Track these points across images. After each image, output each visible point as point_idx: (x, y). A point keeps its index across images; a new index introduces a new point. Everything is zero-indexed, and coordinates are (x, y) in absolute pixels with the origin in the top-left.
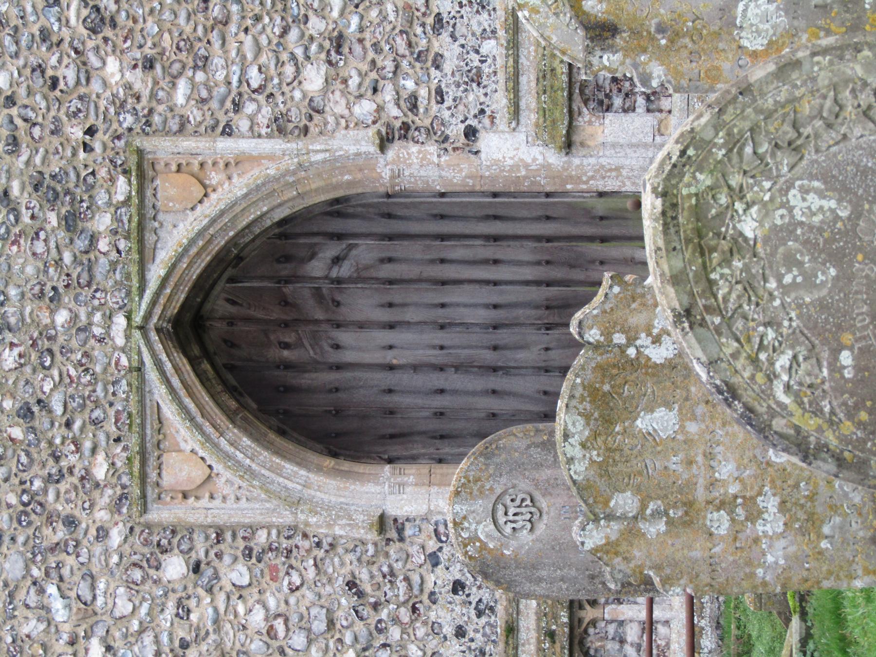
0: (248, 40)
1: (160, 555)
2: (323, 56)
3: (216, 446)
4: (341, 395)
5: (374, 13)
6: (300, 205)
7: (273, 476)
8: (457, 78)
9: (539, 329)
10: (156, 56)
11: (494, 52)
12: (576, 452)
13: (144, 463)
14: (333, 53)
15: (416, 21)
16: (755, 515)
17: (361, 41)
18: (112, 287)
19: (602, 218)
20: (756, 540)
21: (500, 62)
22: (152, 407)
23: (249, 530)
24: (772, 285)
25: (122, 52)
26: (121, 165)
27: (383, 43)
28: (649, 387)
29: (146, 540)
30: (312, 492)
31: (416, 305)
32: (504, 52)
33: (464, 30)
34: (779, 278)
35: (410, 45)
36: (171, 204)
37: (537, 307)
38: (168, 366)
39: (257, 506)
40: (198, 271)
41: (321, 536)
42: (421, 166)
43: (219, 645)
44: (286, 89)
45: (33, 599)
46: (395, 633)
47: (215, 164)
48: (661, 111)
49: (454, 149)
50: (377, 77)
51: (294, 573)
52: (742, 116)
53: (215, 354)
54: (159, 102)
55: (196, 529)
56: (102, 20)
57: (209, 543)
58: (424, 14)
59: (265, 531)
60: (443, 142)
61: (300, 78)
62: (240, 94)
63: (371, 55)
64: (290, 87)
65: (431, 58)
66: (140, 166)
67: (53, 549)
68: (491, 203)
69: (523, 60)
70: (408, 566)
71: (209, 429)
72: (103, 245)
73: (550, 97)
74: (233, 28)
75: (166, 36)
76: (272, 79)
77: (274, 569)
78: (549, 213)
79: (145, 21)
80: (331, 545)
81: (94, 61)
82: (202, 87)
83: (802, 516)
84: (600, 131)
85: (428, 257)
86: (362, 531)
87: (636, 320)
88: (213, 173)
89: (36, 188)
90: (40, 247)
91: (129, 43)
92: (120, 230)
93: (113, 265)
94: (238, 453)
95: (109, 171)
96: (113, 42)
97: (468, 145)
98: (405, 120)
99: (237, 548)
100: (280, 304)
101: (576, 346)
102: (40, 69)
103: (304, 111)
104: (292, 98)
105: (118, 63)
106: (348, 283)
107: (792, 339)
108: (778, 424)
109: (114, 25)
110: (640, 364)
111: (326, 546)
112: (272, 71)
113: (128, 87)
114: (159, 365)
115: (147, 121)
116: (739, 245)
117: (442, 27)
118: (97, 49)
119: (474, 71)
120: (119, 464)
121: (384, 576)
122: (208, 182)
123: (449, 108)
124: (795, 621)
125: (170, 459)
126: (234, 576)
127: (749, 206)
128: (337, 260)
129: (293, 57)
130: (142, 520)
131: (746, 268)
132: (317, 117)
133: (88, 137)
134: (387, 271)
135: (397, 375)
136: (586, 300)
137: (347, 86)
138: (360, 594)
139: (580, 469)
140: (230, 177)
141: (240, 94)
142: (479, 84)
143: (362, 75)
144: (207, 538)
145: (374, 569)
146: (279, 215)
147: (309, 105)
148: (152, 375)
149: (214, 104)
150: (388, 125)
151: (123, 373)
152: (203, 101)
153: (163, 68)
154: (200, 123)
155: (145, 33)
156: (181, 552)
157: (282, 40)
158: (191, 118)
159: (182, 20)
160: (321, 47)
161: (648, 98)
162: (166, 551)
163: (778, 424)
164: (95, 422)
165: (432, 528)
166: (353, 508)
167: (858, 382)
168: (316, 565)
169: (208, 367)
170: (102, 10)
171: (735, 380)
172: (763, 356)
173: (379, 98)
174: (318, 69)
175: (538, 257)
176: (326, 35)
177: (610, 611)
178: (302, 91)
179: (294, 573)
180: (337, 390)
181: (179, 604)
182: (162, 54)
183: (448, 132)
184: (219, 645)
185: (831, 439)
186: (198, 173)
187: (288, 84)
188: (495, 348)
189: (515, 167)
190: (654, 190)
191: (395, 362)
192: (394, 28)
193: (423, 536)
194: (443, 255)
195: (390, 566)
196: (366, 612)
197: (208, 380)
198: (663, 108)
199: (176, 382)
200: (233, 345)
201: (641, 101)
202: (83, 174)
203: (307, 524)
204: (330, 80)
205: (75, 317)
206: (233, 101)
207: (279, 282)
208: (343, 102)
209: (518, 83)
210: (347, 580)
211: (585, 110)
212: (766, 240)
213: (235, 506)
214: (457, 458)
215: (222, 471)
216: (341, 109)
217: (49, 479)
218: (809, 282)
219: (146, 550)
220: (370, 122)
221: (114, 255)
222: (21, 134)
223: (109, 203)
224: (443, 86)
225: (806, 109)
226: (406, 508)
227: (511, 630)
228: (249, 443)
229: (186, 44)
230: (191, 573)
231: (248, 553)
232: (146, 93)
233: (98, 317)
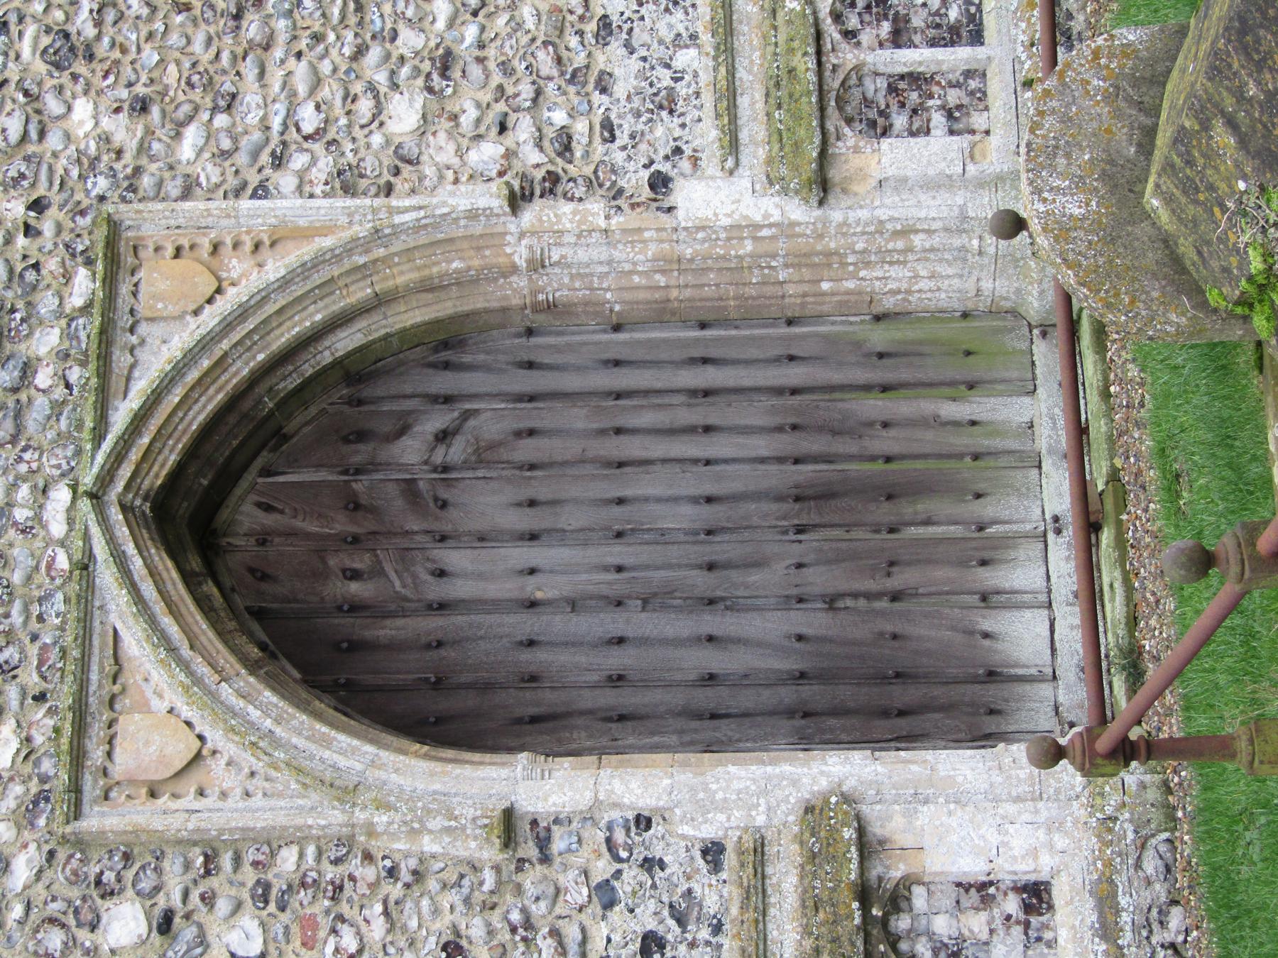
1: (99, 901)
2: (420, 82)
3: (214, 696)
4: (447, 653)
5: (502, 20)
7: (312, 747)
8: (636, 102)
9: (786, 532)
10: (153, 96)
11: (695, 65)
13: (80, 728)
14: (435, 76)
15: (568, 30)
17: (480, 60)
18: (53, 441)
19: (881, 356)
21: (705, 78)
22: (103, 635)
23: (265, 849)
25: (100, 92)
26: (83, 252)
27: (516, 63)
29: (75, 873)
30: (382, 775)
31: (576, 501)
32: (711, 63)
33: (646, 37)
35: (559, 61)
36: (160, 306)
37: (780, 498)
38: (137, 564)
39: (282, 803)
40: (201, 418)
41: (397, 857)
44: (358, 132)
47: (236, 245)
48: (973, 132)
49: (633, 206)
50: (506, 109)
51: (346, 931)
53: (233, 590)
54: (153, 159)
55: (168, 850)
56: (72, 49)
57: (191, 875)
58: (582, 18)
59: (295, 849)
60: (614, 198)
61: (382, 118)
62: (284, 144)
63: (497, 78)
64: (366, 131)
65: (592, 80)
66: (111, 243)
68: (697, 340)
69: (741, 73)
70: (558, 910)
71: (202, 669)
72: (43, 378)
73: (788, 111)
74: (278, 53)
75: (172, 68)
76: (337, 120)
77: (309, 924)
78: (793, 352)
79: (139, 50)
80: (415, 873)
81: (53, 105)
82: (222, 135)
84: (873, 163)
85: (595, 426)
86: (473, 844)
88: (234, 261)
91: (111, 79)
92: (73, 352)
93: (57, 408)
94: (251, 709)
95: (63, 259)
96: (85, 79)
97: (655, 200)
98: (552, 168)
99: (243, 884)
100: (346, 508)
103: (386, 163)
104: (368, 146)
105: (91, 106)
106: (461, 469)
109: (90, 57)
111: (406, 876)
112: (338, 110)
113: (106, 139)
115: (131, 185)
117: (611, 33)
118: (60, 89)
119: (664, 93)
120: (39, 739)
121: (514, 930)
122: (224, 275)
123: (624, 148)
125: (130, 725)
129: (372, 88)
130: (68, 829)
132: (406, 170)
133: (32, 214)
134: (527, 450)
135: (545, 618)
137: (457, 125)
141: (284, 144)
142: (671, 112)
143: (483, 108)
144: (187, 866)
145: (495, 918)
147: (395, 152)
148: (106, 575)
149: (242, 159)
150: (524, 176)
151: (58, 582)
152: (226, 155)
153: (163, 112)
154: (218, 186)
155: (138, 66)
156: (138, 894)
157: (354, 66)
158: (203, 180)
159: (197, 47)
160: (417, 71)
161: (950, 115)
162: (112, 893)
165: (601, 836)
166: (454, 800)
168: (386, 913)
169: (215, 590)
170: (74, 37)
173: (509, 140)
174: (411, 101)
175: (778, 420)
176: (425, 54)
178: (384, 135)
179: (346, 931)
180: (440, 644)
182: (163, 94)
183: (622, 183)
187: (362, 127)
188: (711, 567)
191: (539, 595)
192: (533, 40)
193: (586, 852)
194: (620, 422)
195: (524, 910)
197: (212, 609)
198: (976, 127)
199: (148, 589)
200: (265, 577)
201: (938, 119)
202: (19, 267)
203: (371, 832)
204: (429, 118)
206: (273, 154)
207: (346, 472)
208: (451, 148)
209: (735, 106)
210: (444, 939)
211: (847, 130)
213: (240, 805)
215: (220, 745)
216: (447, 155)
219: (75, 893)
220: (494, 174)
221: (59, 393)
223: (59, 313)
224: (613, 116)
226: (554, 799)
228: (275, 699)
230: (155, 933)
231: (262, 893)
232: (131, 146)
233: (24, 491)
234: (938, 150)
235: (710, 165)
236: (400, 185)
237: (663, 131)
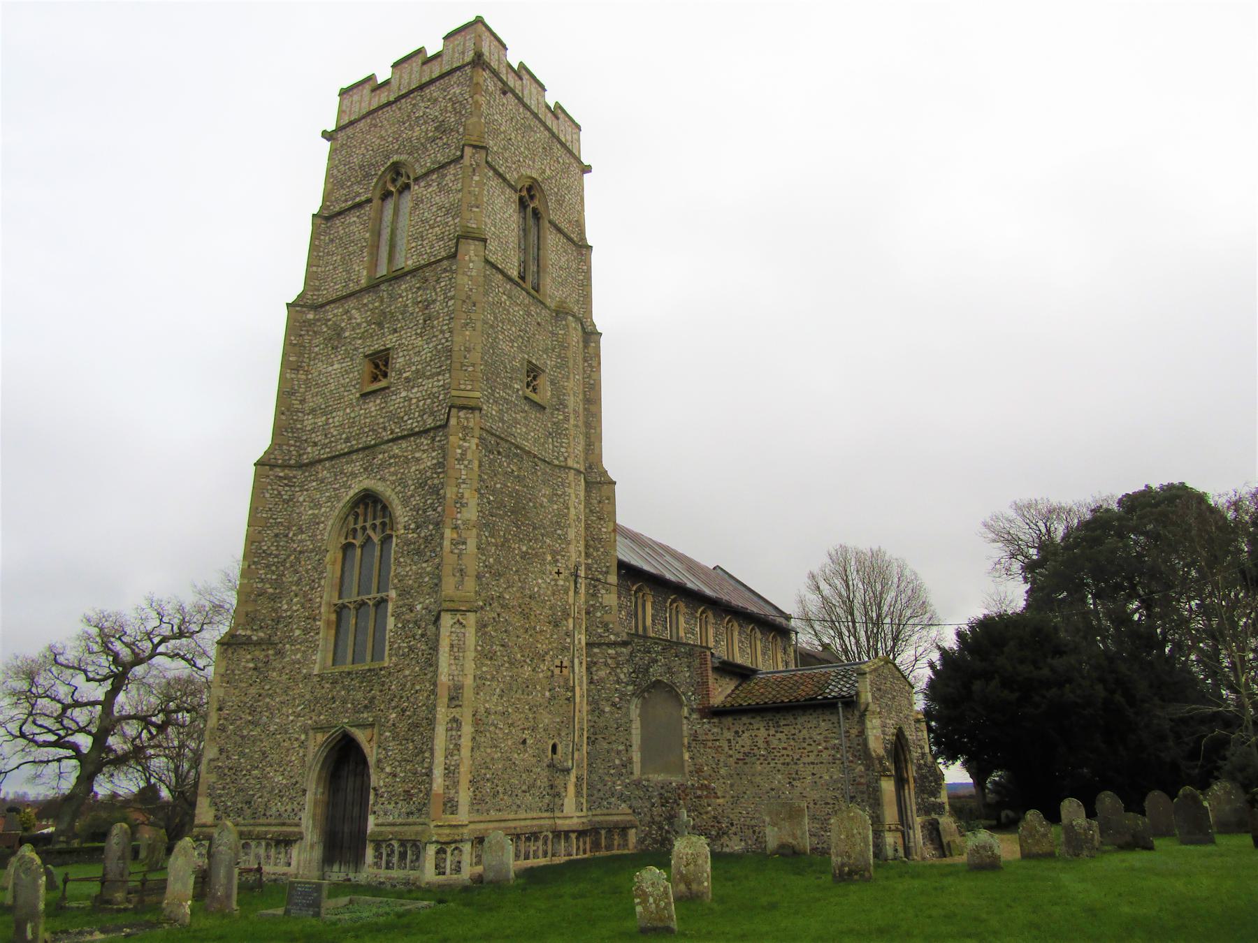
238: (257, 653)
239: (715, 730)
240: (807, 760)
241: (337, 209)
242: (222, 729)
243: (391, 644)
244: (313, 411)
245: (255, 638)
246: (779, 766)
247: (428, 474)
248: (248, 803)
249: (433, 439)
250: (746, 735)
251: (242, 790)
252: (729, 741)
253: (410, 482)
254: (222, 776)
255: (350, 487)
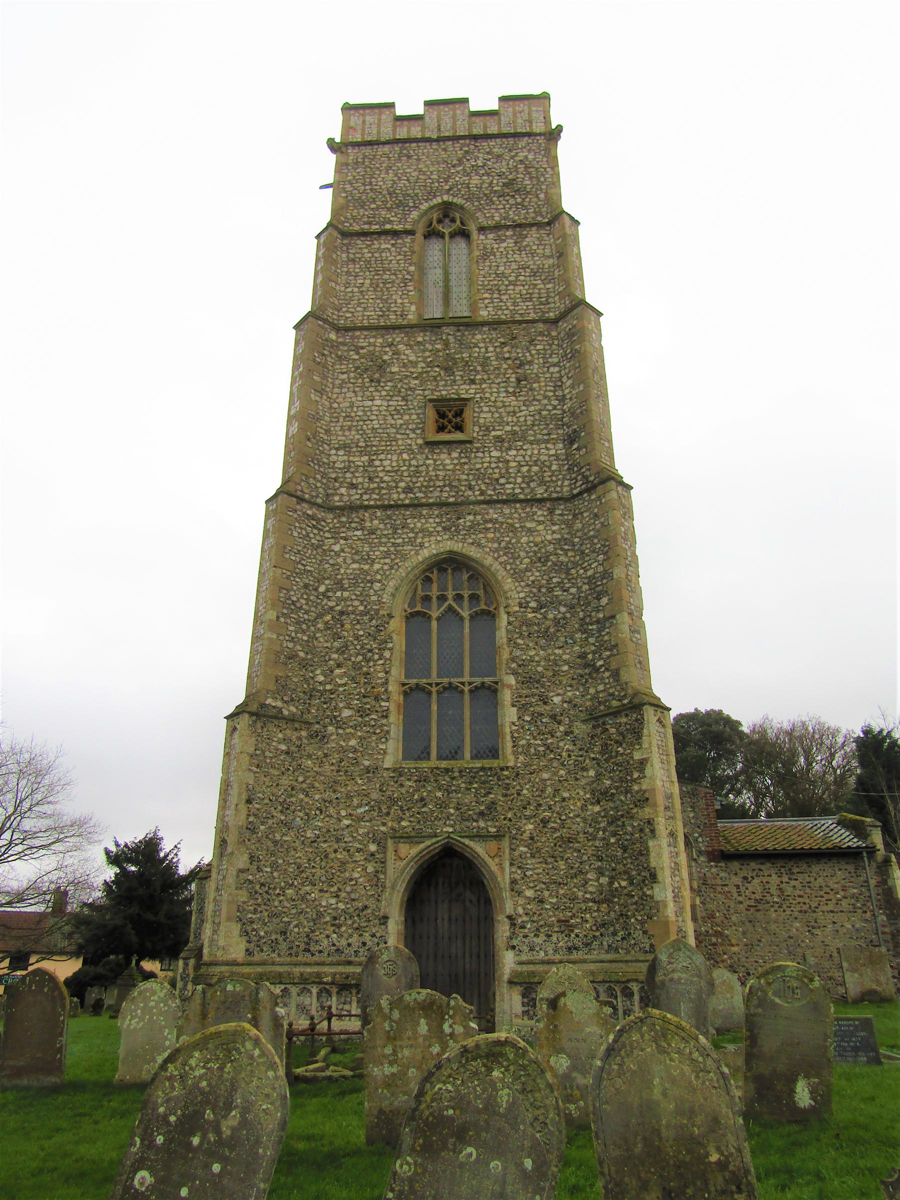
0: (540, 871)
5: (551, 913)
6: (488, 888)
12: (413, 997)
16: (391, 1064)
20: (382, 1064)
21: (537, 958)
24: (476, 1083)
28: (435, 1024)
34: (478, 1085)
42: (503, 930)
43: (348, 862)
45: (364, 802)
46: (350, 922)
52: (534, 1070)
67: (380, 808)
72: (475, 824)
81: (532, 821)
83: (390, 1082)
87: (457, 1018)
89: (492, 803)
90: (474, 804)
93: (468, 827)
101: (449, 996)
102: (529, 804)
107: (457, 1091)
108: (428, 1085)
109: (544, 827)
110: (443, 1020)
113: (524, 832)
114: (437, 842)
116: (490, 1070)
124: (351, 1073)
125: (407, 846)
126: (369, 867)
127: (503, 1073)
128: (471, 901)
131: (481, 1072)
136: (464, 1001)
138: (363, 910)
139: (407, 998)
140: (498, 865)
143: (531, 909)
146: (485, 882)
148: (434, 840)
149: (520, 860)
163: (428, 1085)
164: (419, 822)
167: (443, 1116)
171: (443, 1069)
172: (451, 1079)
177: (354, 998)
181: (361, 849)
184: (348, 862)
185: (423, 1106)
186: (498, 855)
189: (503, 963)
190: (507, 1037)
196: (357, 912)
199: (432, 848)
201: (526, 1009)
205: (452, 815)
212: (491, 1080)
214: (406, 946)
217: (401, 807)
218: (477, 1097)
222: (509, 798)
225: (537, 1095)
227: (350, 963)
229: (539, 850)
231: (377, 872)
234: (518, 1008)
235: (517, 958)
236: (513, 893)
237: (525, 948)
238: (288, 732)
239: (722, 874)
240: (825, 908)
241: (356, 228)
242: (252, 829)
243: (515, 740)
244: (344, 446)
245: (286, 713)
246: (796, 914)
247: (550, 548)
248: (284, 933)
249: (551, 512)
250: (756, 881)
251: (276, 915)
252: (738, 887)
253: (522, 554)
254: (253, 894)
255: (421, 545)
